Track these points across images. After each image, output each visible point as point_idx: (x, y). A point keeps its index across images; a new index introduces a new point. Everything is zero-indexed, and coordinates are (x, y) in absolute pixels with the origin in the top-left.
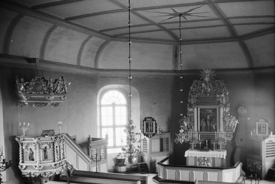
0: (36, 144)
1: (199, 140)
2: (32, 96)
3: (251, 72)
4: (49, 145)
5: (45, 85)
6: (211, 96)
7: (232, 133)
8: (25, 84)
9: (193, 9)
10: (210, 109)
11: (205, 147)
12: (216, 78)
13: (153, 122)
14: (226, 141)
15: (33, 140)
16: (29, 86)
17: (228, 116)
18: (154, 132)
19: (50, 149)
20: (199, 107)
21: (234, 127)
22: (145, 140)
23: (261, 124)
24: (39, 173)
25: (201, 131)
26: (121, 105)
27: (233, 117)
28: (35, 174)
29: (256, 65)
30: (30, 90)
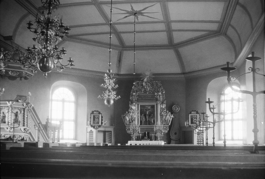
0: (9, 108)
1: (140, 132)
2: (10, 65)
3: (183, 76)
4: (20, 110)
5: (22, 55)
6: (150, 94)
7: (168, 126)
8: (4, 53)
9: (147, 7)
10: (149, 106)
11: (145, 137)
12: (155, 79)
13: (196, 114)
14: (163, 133)
15: (6, 104)
16: (8, 55)
17: (165, 112)
18: (100, 124)
19: (21, 114)
20: (140, 103)
21: (170, 121)
22: (91, 132)
23: (193, 116)
24: (9, 134)
25: (141, 124)
26: (69, 102)
27: (169, 112)
28: (6, 136)
29: (187, 70)
30: (8, 58)
